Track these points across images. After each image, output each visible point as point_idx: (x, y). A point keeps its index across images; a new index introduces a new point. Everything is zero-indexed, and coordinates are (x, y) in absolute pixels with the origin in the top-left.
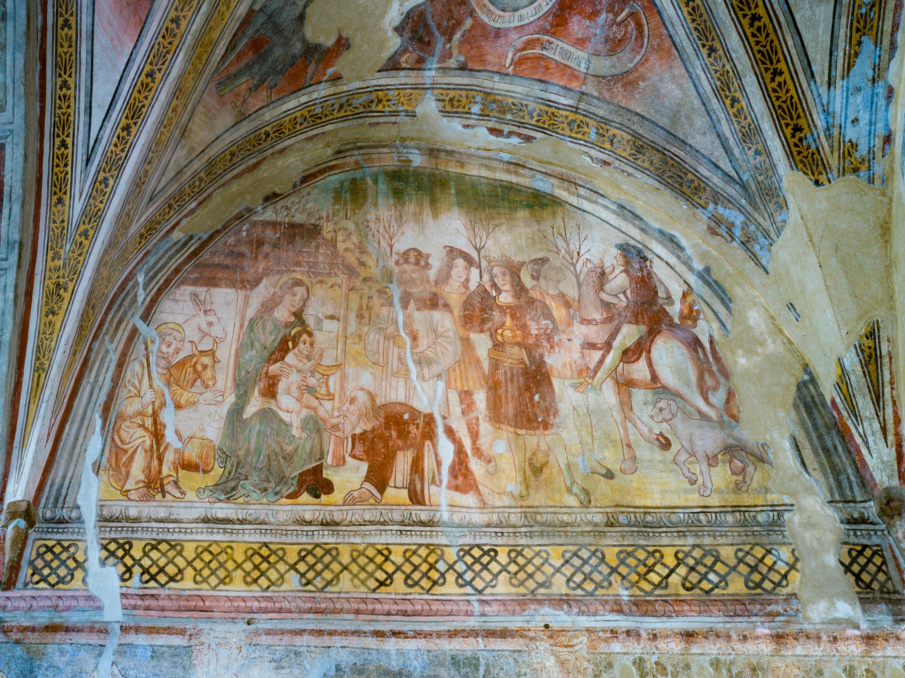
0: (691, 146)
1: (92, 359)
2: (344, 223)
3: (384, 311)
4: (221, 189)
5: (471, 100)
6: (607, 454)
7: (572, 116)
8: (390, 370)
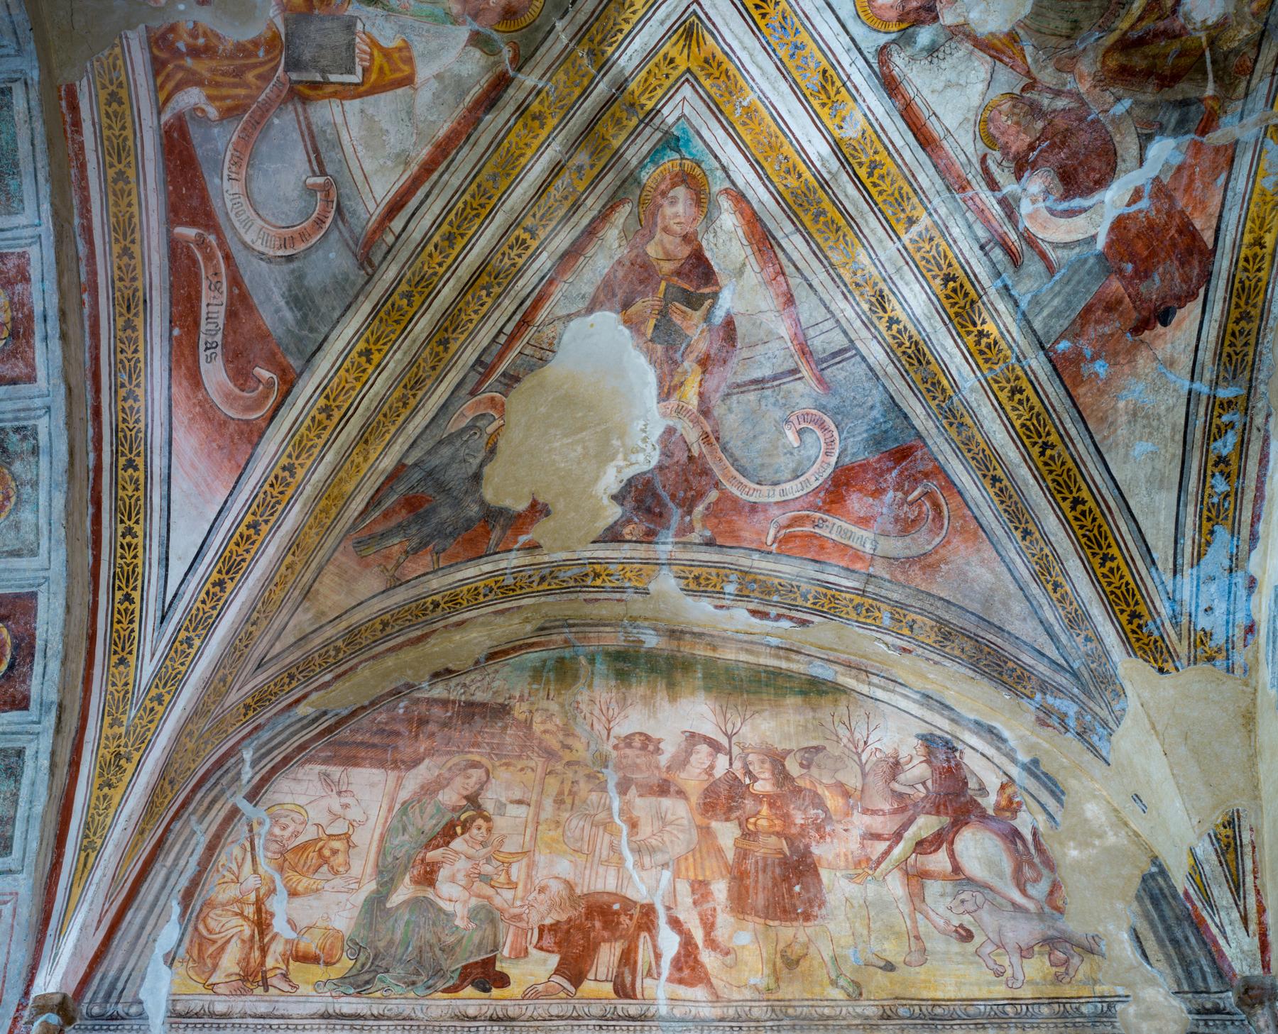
0: (1009, 633)
1: (170, 841)
2: (544, 704)
3: (594, 797)
4: (371, 662)
7: (858, 600)
8: (596, 858)
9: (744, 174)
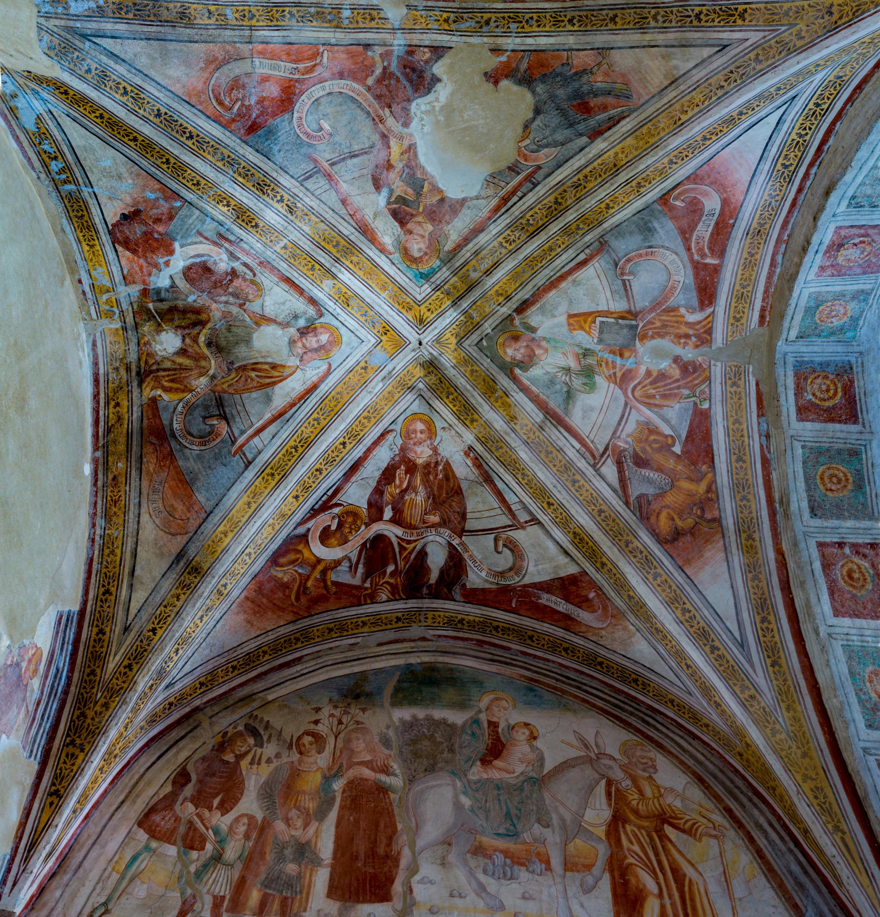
5: (352, 20)
7: (254, 22)
9: (382, 261)
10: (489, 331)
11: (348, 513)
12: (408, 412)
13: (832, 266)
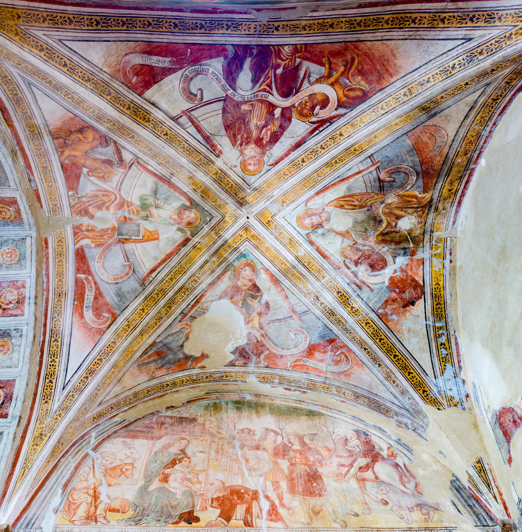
3: (231, 450)
6: (354, 506)
7: (323, 385)
9: (267, 264)
10: (205, 227)
11: (306, 116)
12: (258, 176)
13: (18, 288)
